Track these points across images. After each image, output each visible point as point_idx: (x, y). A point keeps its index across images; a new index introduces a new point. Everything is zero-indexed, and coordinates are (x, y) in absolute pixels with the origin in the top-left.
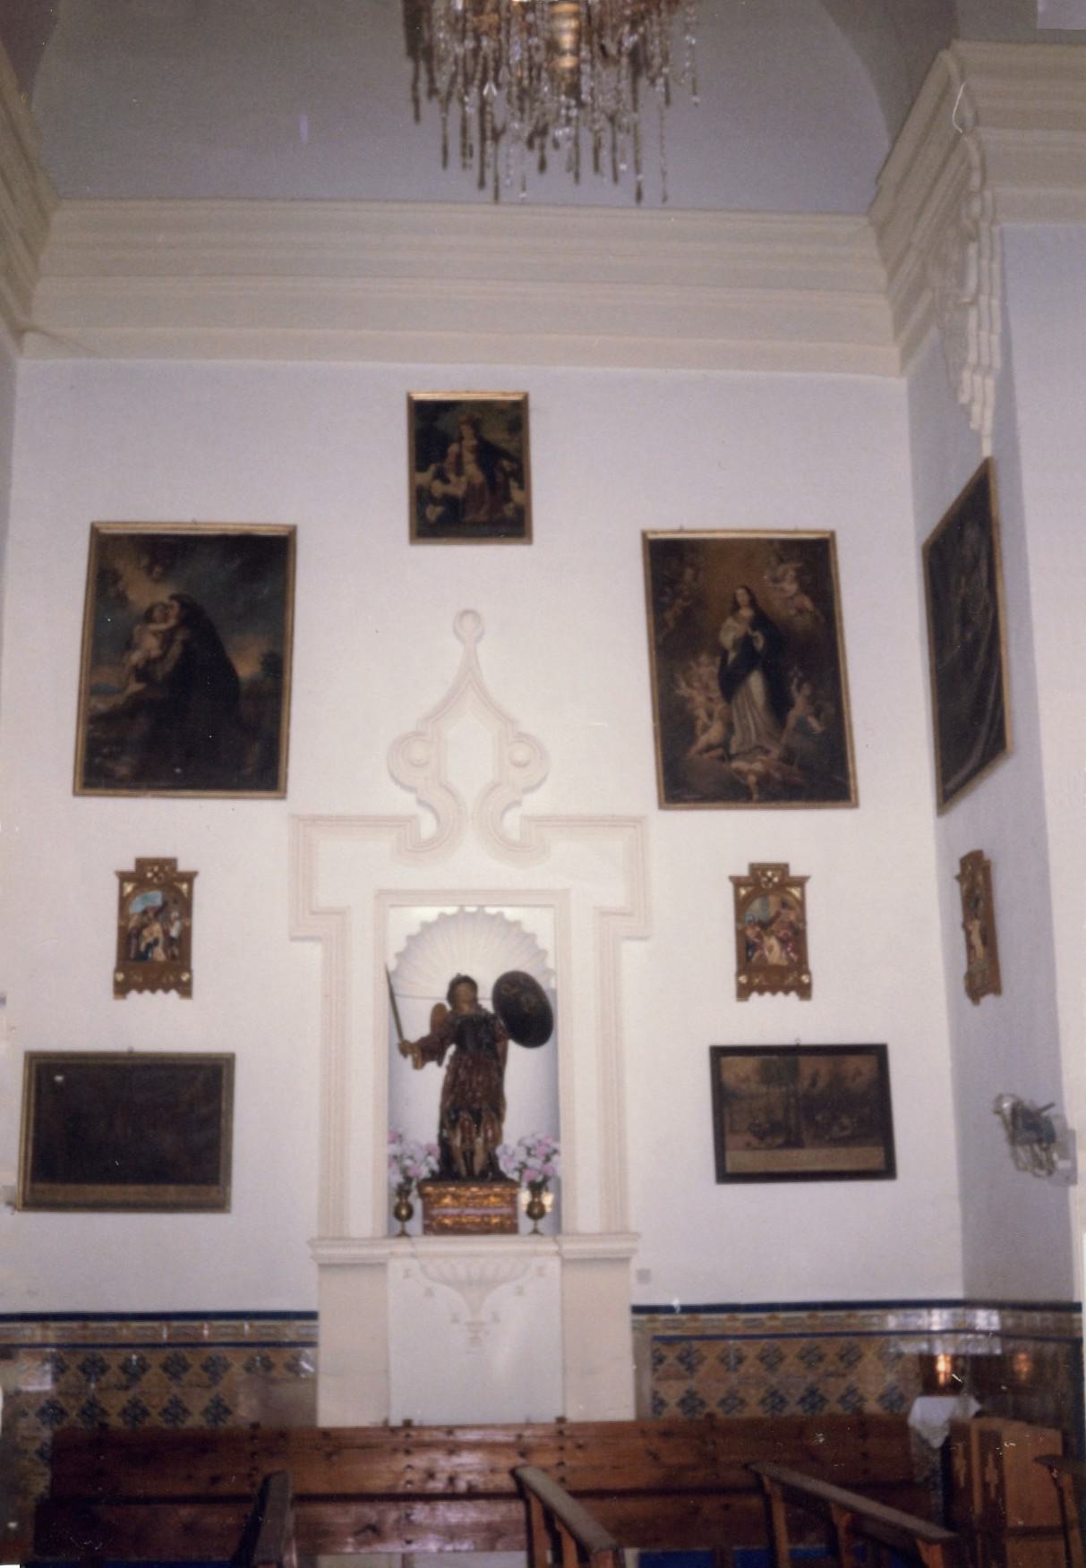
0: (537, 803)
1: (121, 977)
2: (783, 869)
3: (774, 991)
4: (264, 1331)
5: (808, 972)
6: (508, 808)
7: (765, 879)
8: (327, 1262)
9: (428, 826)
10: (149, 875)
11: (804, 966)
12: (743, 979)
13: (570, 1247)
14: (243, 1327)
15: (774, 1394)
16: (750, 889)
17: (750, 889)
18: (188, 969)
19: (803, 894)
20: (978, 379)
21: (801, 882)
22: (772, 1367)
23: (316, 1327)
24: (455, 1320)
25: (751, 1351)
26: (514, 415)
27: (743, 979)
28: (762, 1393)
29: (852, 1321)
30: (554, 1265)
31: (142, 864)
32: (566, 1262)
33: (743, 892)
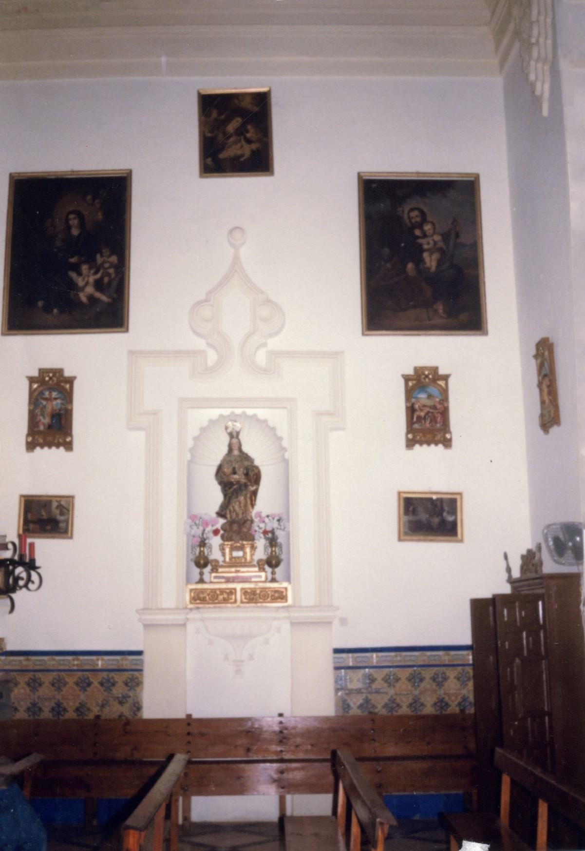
0: (274, 343)
1: (30, 439)
2: (435, 370)
3: (429, 444)
4: (38, 663)
5: (450, 432)
6: (258, 348)
7: (423, 377)
8: (149, 623)
9: (212, 357)
10: (47, 379)
11: (447, 429)
12: (410, 436)
13: (296, 614)
14: (372, 657)
15: (441, 701)
16: (414, 382)
17: (414, 382)
18: (71, 435)
19: (447, 384)
20: (540, 65)
21: (446, 378)
22: (440, 685)
23: (334, 663)
24: (226, 658)
25: (404, 674)
26: (262, 100)
27: (410, 436)
28: (435, 699)
29: (125, 663)
30: (286, 626)
31: (42, 371)
32: (295, 624)
33: (410, 384)
